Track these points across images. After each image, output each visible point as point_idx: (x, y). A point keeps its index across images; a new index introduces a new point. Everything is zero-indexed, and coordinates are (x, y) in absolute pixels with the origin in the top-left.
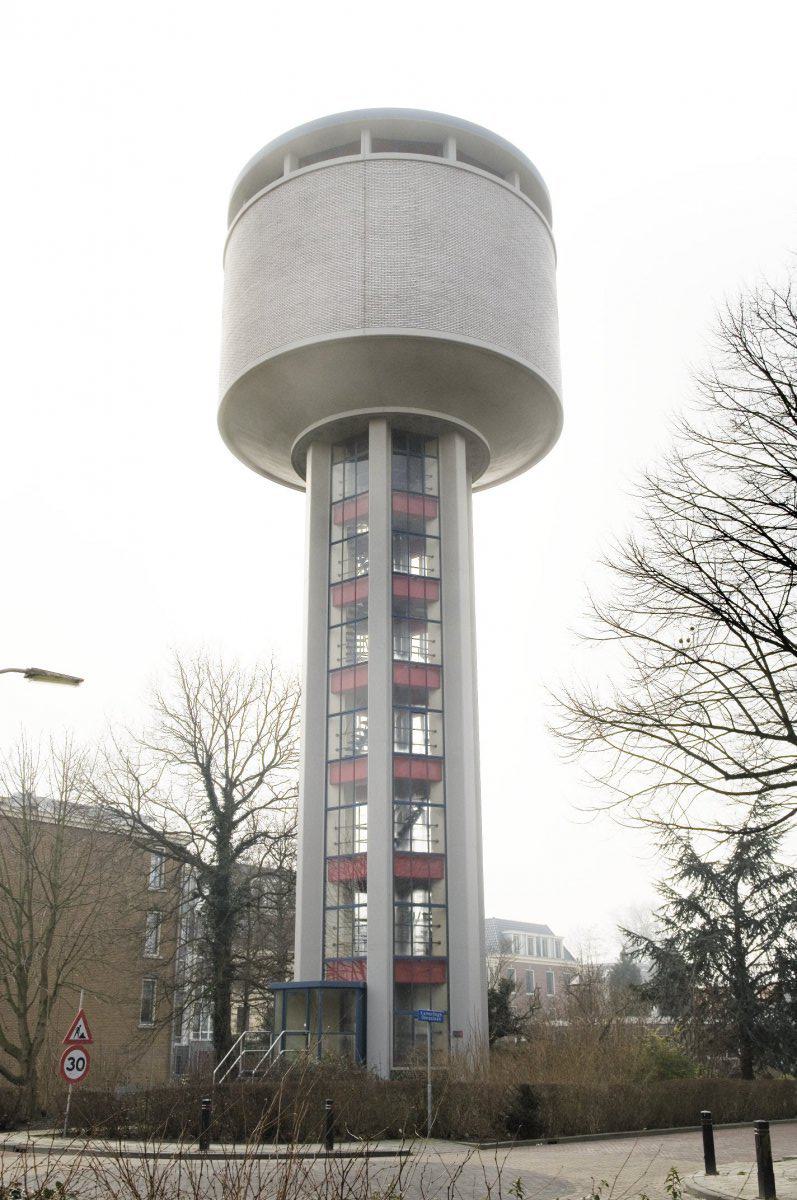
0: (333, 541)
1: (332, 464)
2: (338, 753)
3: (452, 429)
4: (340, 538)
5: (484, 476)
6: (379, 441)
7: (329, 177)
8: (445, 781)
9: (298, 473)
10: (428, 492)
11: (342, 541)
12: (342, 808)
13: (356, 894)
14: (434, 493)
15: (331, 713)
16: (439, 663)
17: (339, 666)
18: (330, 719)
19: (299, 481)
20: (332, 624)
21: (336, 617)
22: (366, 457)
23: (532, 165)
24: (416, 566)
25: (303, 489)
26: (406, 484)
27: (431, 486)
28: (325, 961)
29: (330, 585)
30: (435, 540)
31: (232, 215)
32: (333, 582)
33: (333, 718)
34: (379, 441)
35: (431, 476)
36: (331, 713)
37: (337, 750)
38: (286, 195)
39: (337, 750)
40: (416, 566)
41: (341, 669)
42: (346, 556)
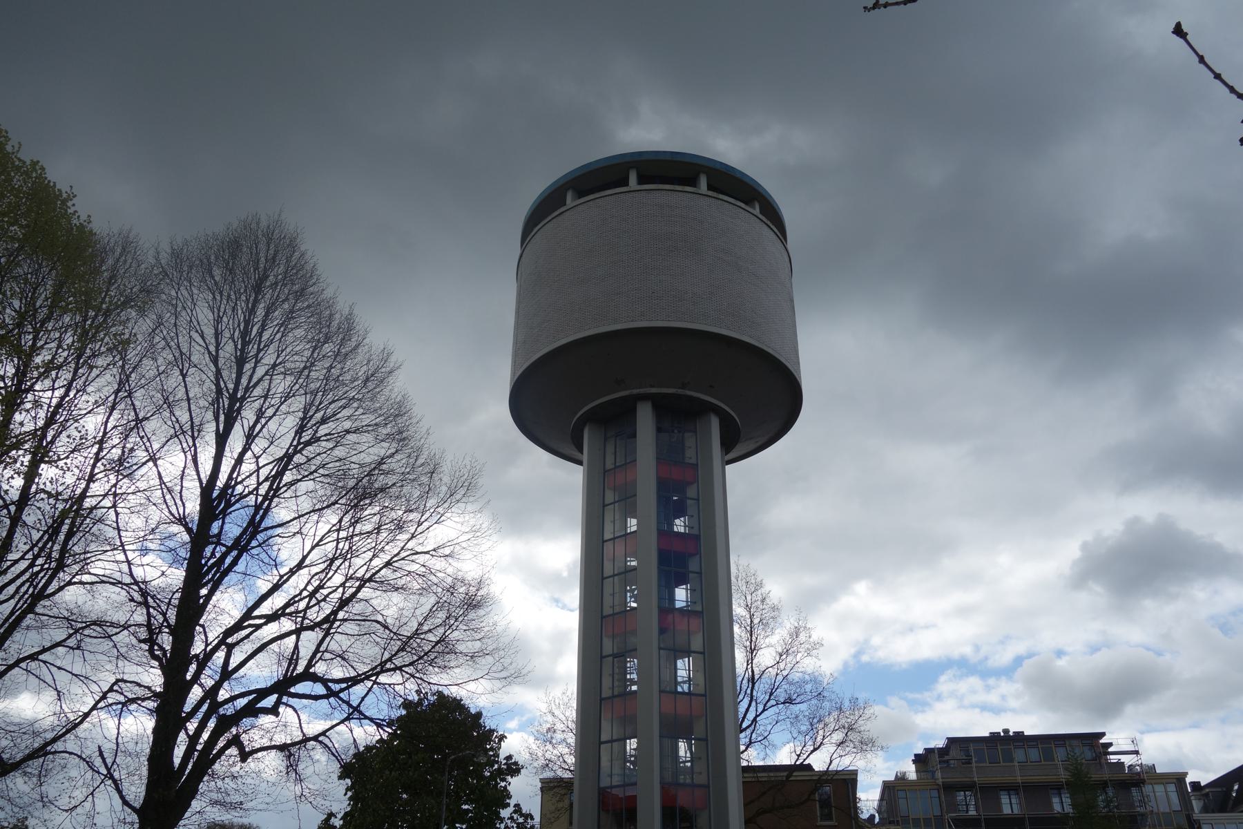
0: (605, 576)
1: (605, 440)
2: (611, 691)
3: (705, 409)
4: (612, 501)
5: (737, 446)
6: (645, 419)
7: (607, 203)
8: (701, 554)
9: (577, 448)
10: (687, 461)
11: (614, 503)
12: (616, 741)
13: (629, 519)
14: (693, 461)
15: (604, 654)
16: (695, 463)
17: (612, 613)
18: (605, 581)
19: (576, 455)
20: (606, 502)
21: (610, 497)
22: (634, 435)
23: (752, 179)
24: (680, 525)
25: (580, 463)
26: (669, 456)
27: (690, 454)
28: (599, 788)
29: (603, 617)
30: (696, 575)
31: (522, 246)
32: (605, 614)
33: (608, 507)
34: (645, 419)
35: (690, 448)
36: (604, 654)
37: (611, 595)
38: (547, 231)
39: (611, 595)
40: (680, 525)
41: (614, 614)
42: (617, 517)
